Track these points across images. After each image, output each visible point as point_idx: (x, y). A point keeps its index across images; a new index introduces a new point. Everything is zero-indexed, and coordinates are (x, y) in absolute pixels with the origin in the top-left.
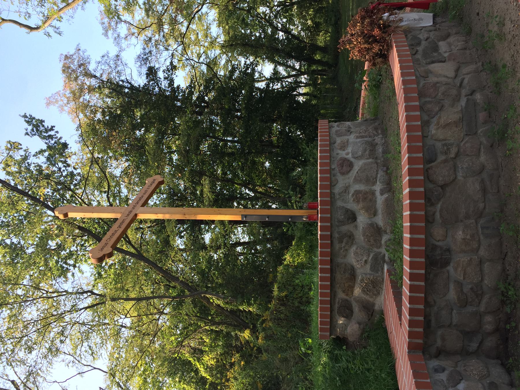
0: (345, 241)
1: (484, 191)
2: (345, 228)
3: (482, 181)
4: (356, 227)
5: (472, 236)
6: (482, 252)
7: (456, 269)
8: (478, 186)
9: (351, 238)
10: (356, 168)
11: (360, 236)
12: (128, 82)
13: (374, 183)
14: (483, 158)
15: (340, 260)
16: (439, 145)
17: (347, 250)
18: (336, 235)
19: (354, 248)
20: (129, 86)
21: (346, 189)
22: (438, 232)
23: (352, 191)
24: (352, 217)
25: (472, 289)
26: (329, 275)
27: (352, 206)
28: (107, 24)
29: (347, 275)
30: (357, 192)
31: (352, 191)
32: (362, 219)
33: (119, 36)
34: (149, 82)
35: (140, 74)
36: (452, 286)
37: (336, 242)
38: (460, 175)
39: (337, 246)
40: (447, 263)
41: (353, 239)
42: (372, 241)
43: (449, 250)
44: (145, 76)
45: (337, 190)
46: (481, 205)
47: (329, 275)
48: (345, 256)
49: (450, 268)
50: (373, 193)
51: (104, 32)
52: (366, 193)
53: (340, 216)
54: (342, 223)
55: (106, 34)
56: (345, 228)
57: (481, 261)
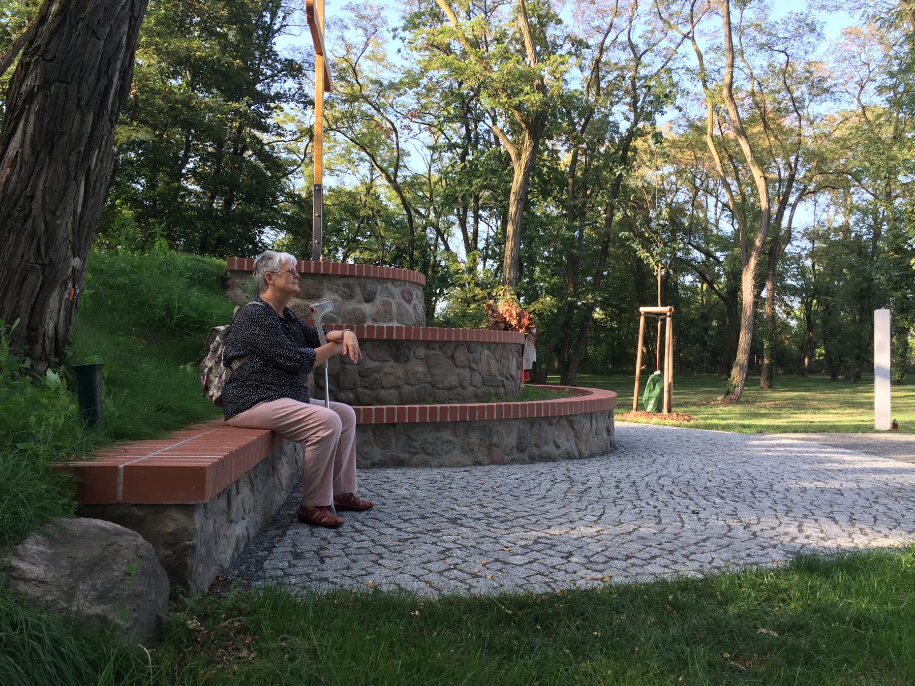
0: (346, 290)
1: (450, 389)
2: (358, 291)
3: (456, 388)
4: (360, 302)
5: (419, 379)
6: (407, 387)
7: (392, 367)
8: (453, 383)
9: (350, 296)
10: (408, 306)
11: (351, 305)
12: (282, 26)
13: (398, 321)
14: (470, 388)
15: (325, 284)
16: (477, 355)
17: (337, 291)
18: (351, 281)
19: (340, 299)
20: (276, 27)
21: (391, 295)
22: (421, 352)
23: (391, 300)
24: (369, 299)
25: (377, 380)
26: (312, 271)
27: (378, 300)
28: (365, 13)
29: (312, 291)
30: (390, 304)
31: (391, 300)
32: (367, 308)
33: (346, 27)
34: (280, 62)
35: (294, 49)
36: (378, 364)
37: (345, 281)
38: (461, 371)
39: (341, 282)
40: (397, 360)
41: (347, 299)
42: (349, 317)
43: (408, 360)
44: (289, 58)
45: (389, 285)
46: (440, 386)
47: (312, 271)
48: (330, 290)
49: (392, 363)
50: (391, 320)
51: (354, 4)
52: (390, 313)
53: (370, 287)
54: (364, 288)
55: (350, 8)
56: (358, 291)
57: (398, 387)
